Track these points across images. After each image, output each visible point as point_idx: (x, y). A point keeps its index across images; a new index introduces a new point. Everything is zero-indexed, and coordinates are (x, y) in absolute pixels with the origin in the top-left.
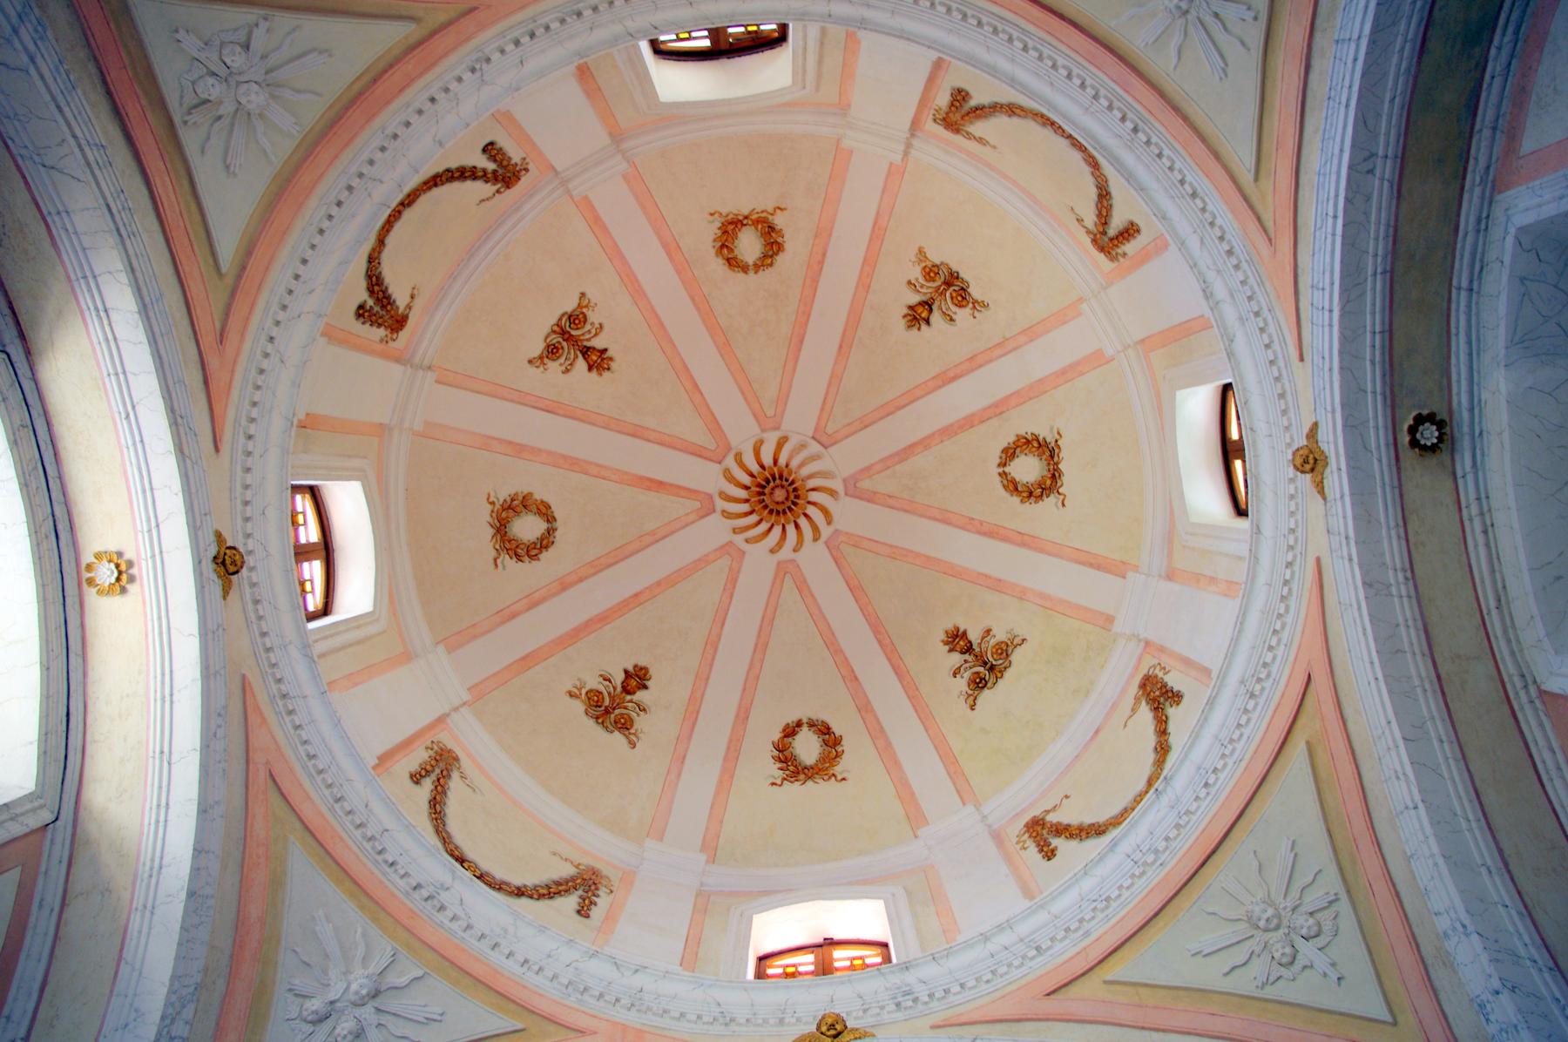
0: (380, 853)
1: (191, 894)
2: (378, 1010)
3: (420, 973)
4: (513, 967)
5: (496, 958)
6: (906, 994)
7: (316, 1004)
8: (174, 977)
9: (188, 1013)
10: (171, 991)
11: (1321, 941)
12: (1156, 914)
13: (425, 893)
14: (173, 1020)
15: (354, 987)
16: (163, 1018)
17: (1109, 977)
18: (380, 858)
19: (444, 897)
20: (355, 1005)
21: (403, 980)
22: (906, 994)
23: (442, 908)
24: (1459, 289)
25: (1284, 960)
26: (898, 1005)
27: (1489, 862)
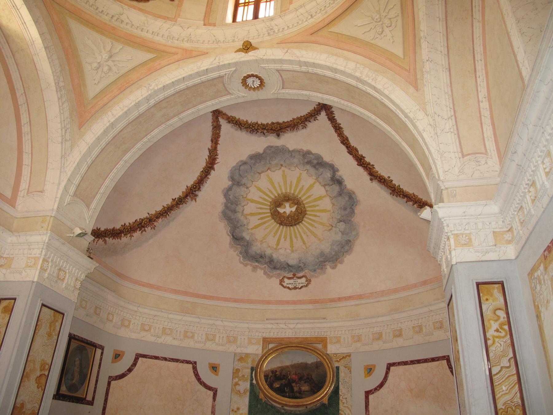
0: (97, 9)
1: (45, 48)
2: (113, 61)
3: (121, 47)
4: (149, 36)
5: (144, 34)
6: (271, 29)
7: (95, 65)
8: (53, 72)
9: (61, 79)
10: (54, 76)
11: (391, 28)
12: (346, 10)
13: (115, 18)
14: (58, 83)
15: (104, 57)
16: (55, 84)
17: (330, 30)
18: (97, 11)
19: (122, 17)
20: (106, 62)
21: (117, 51)
22: (271, 29)
23: (122, 21)
24: (126, 162)
25: (379, 33)
26: (269, 33)
27: (441, 17)
